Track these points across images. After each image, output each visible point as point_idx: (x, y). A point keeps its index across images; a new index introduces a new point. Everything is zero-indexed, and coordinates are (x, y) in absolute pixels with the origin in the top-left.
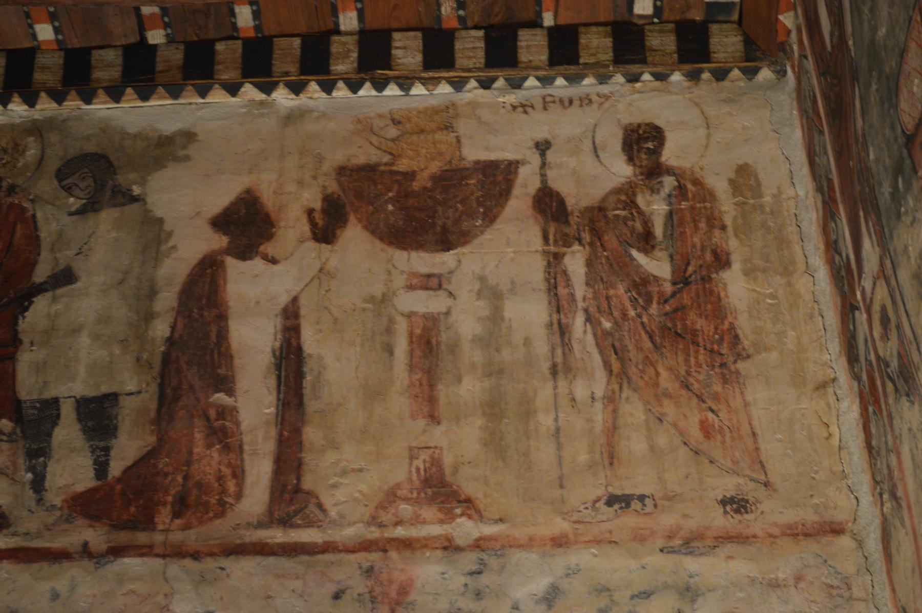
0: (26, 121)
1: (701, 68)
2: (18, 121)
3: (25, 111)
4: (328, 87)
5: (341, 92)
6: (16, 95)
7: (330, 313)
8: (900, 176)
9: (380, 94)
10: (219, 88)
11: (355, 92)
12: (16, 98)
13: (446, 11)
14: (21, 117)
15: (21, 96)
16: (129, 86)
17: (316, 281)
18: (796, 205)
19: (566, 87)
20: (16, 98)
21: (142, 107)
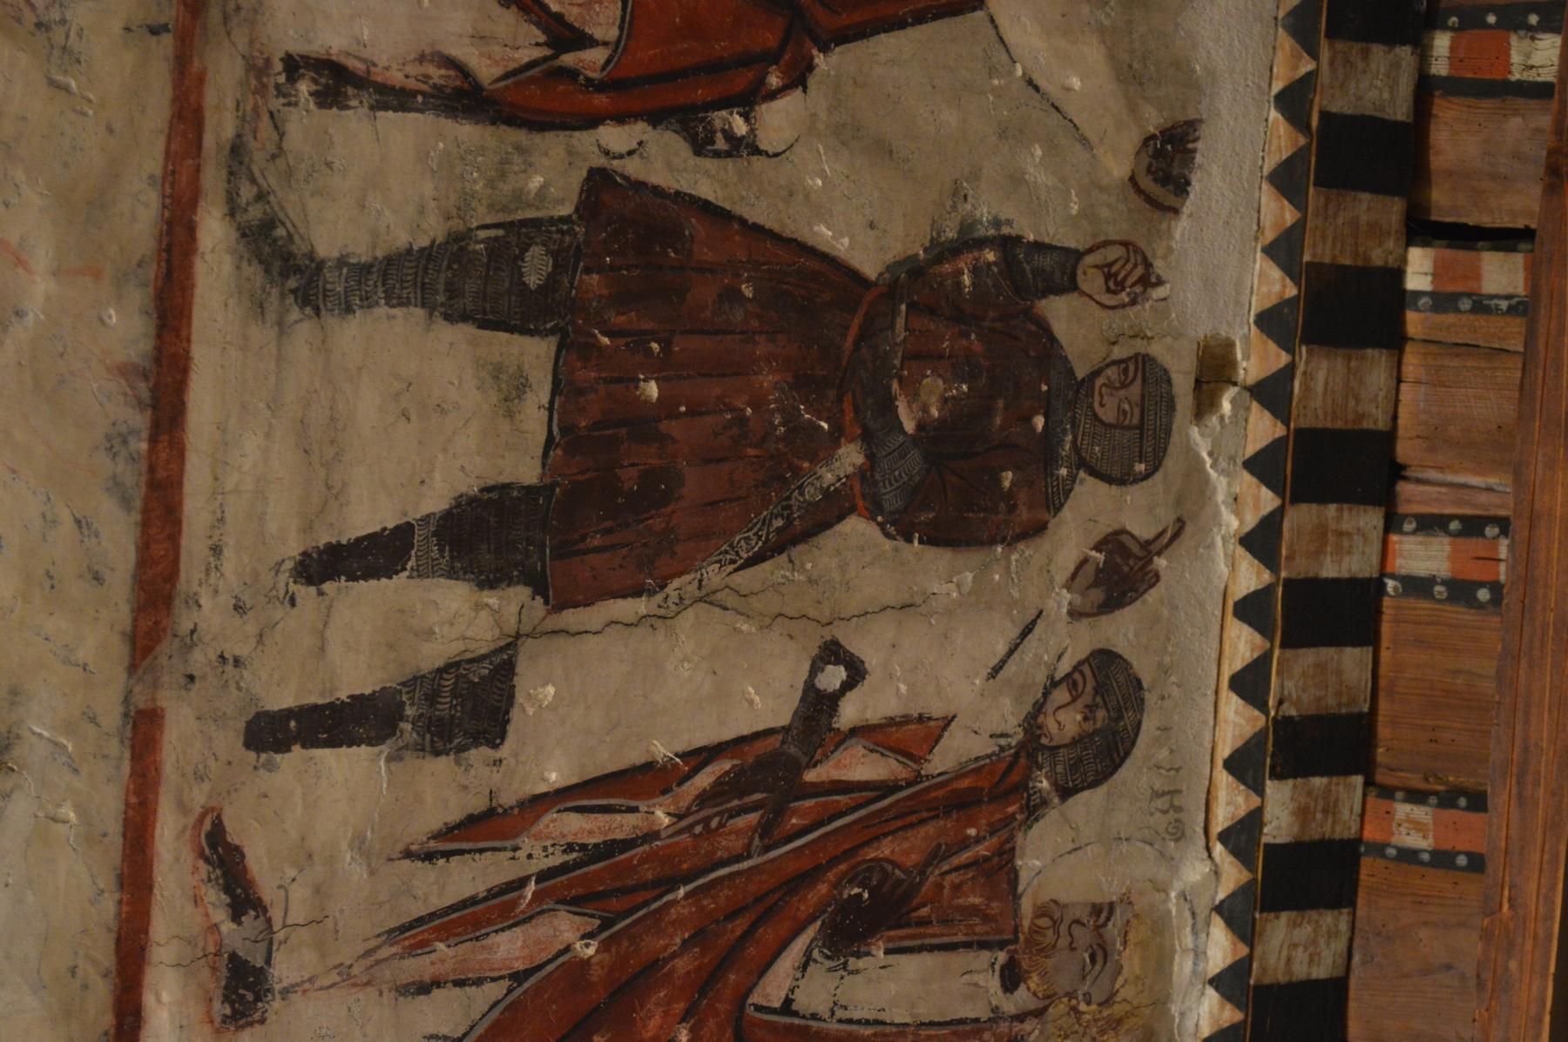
0: (1172, 1030)
1: (1274, 631)
2: (1174, 1009)
3: (1197, 1026)
4: (1243, 765)
5: (1220, 948)
6: (1238, 1016)
7: (520, 621)
8: (654, 400)
9: (1219, 763)
10: (1252, 656)
11: (1230, 765)
12: (1231, 1015)
13: (1418, 826)
14: (1182, 1014)
15: (1234, 1028)
16: (1246, 1015)
17: (712, 598)
18: (214, 754)
19: (1213, 899)
20: (1231, 1015)
21: (1249, 311)
